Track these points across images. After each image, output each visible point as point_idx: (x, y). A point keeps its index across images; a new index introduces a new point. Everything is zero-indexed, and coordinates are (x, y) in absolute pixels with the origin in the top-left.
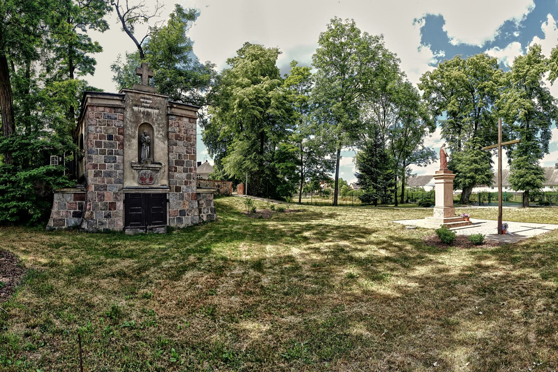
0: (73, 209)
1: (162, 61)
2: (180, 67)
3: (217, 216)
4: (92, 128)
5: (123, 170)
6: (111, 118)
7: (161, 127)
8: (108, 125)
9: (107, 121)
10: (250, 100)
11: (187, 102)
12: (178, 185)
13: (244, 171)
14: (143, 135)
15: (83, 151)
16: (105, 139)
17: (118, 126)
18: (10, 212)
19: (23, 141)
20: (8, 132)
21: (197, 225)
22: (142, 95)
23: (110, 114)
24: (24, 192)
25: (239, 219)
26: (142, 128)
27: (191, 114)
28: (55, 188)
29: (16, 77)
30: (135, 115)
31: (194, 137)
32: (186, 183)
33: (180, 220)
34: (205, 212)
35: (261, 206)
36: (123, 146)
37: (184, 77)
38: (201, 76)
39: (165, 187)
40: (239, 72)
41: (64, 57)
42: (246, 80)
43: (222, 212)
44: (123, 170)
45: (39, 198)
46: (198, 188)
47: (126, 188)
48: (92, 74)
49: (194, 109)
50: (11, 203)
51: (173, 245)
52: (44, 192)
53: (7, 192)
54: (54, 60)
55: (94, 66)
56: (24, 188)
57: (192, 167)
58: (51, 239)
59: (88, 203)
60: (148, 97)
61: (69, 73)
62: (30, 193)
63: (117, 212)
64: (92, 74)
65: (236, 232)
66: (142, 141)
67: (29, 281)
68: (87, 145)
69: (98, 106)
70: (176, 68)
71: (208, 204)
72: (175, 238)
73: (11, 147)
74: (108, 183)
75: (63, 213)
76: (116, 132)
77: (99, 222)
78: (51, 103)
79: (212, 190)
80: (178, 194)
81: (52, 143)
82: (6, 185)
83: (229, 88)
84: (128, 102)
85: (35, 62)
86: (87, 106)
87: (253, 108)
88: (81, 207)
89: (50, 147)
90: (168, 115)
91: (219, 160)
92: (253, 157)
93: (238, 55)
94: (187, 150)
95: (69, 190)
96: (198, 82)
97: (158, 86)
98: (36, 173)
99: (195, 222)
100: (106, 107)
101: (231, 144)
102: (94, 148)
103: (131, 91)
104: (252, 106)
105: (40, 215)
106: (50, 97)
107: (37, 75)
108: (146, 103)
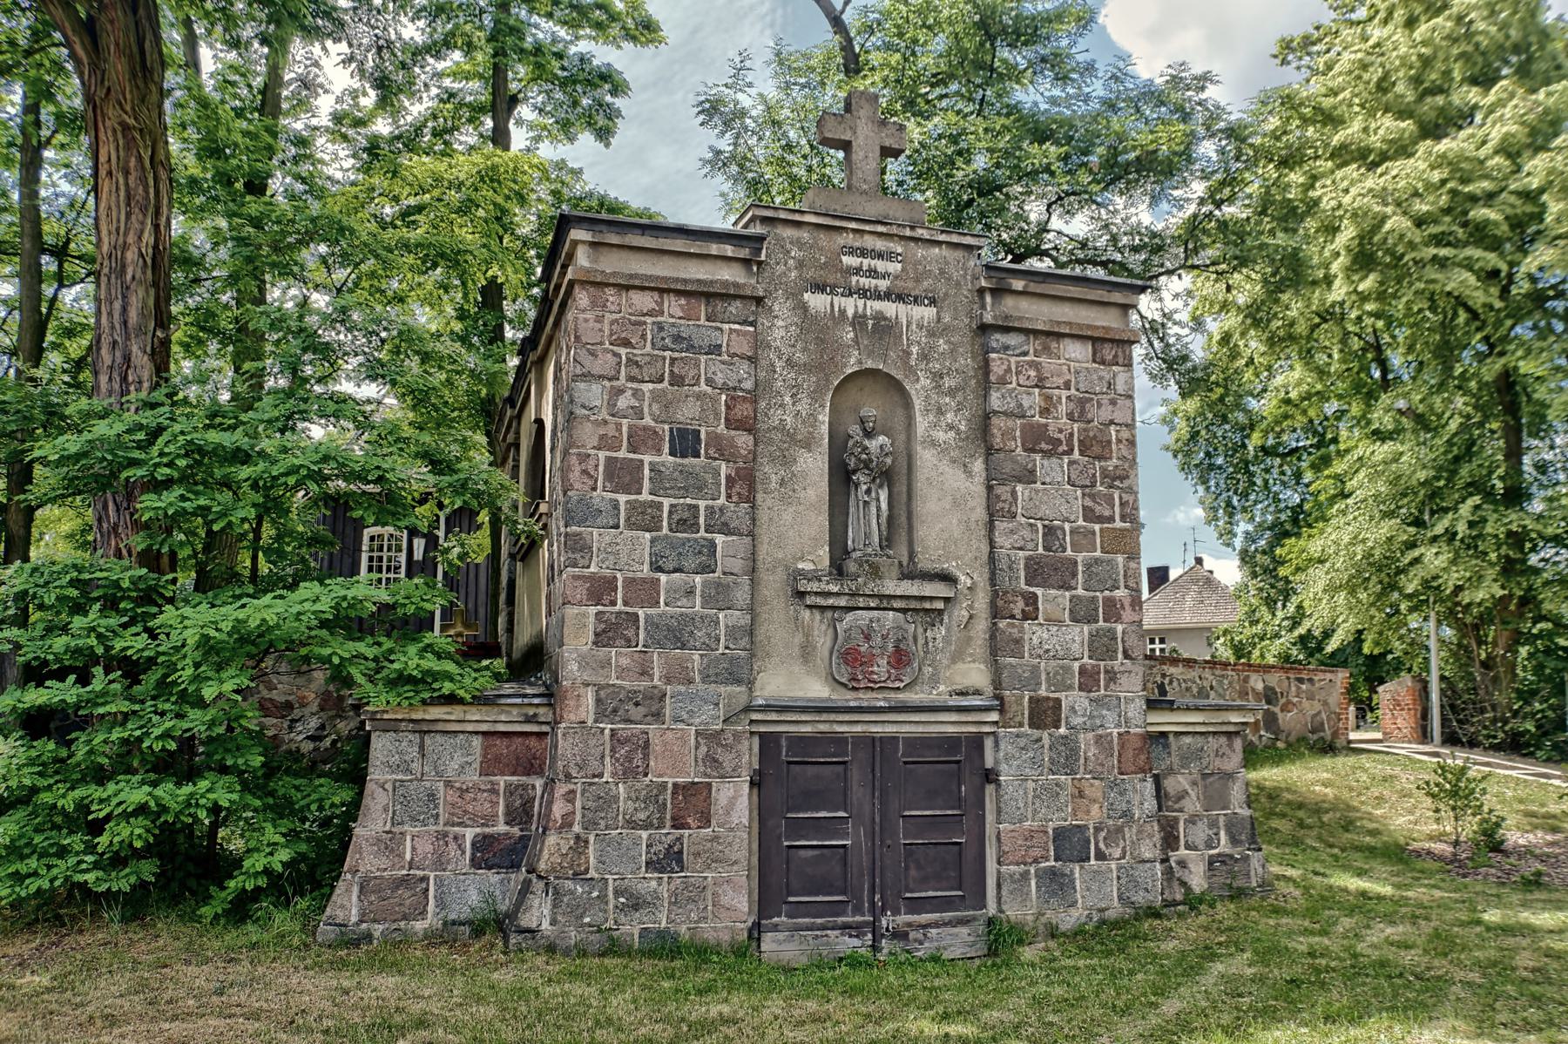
0: (475, 820)
1: (943, 83)
2: (1036, 104)
3: (1266, 864)
4: (593, 394)
5: (751, 610)
6: (689, 349)
7: (952, 392)
8: (677, 380)
9: (673, 360)
10: (1419, 222)
11: (1079, 262)
12: (1043, 692)
13: (1411, 610)
14: (855, 429)
15: (543, 508)
16: (659, 452)
17: (725, 388)
18: (103, 840)
19: (214, 436)
20: (124, 379)
21: (1153, 913)
22: (849, 239)
23: (686, 328)
24: (196, 720)
25: (1397, 886)
26: (853, 392)
27: (1103, 320)
28: (380, 701)
29: (204, 103)
30: (814, 329)
31: (1125, 434)
32: (1088, 680)
33: (1057, 884)
34: (1200, 843)
35: (1533, 815)
36: (752, 489)
37: (1057, 143)
38: (1139, 134)
39: (976, 701)
40: (1347, 94)
41: (469, 48)
42: (1388, 126)
43: (1297, 842)
44: (751, 610)
45: (280, 762)
46: (1152, 705)
47: (766, 708)
48: (604, 134)
49: (1117, 297)
50: (111, 787)
51: (1017, 1027)
52: (314, 723)
53: (84, 723)
54: (418, 53)
55: (618, 102)
56: (201, 704)
57: (1121, 593)
58: (346, 992)
59: (561, 789)
60: (880, 245)
61: (489, 123)
62: (230, 729)
63: (715, 839)
64: (604, 134)
65: (1383, 964)
66: (852, 463)
68: (565, 478)
69: (628, 288)
70: (1012, 110)
71: (1213, 798)
72: (1032, 984)
73: (134, 463)
74: (668, 680)
75: (416, 843)
76: (717, 415)
77: (617, 893)
78: (385, 257)
79: (1235, 718)
80: (1046, 741)
81: (376, 461)
82: (84, 679)
83: (1296, 177)
84: (781, 268)
85: (317, 45)
86: (571, 284)
87: (1441, 263)
88: (521, 813)
89: (361, 477)
90: (984, 329)
91: (1269, 551)
92: (1462, 529)
93: (1333, 15)
94: (1089, 503)
95: (456, 712)
96: (1128, 164)
97: (929, 193)
98: (272, 619)
99: (1140, 898)
100: (669, 291)
101: (1326, 461)
102: (601, 496)
103: (797, 217)
104: (1433, 251)
105: (284, 855)
106: (383, 225)
107: (325, 105)
108: (873, 273)
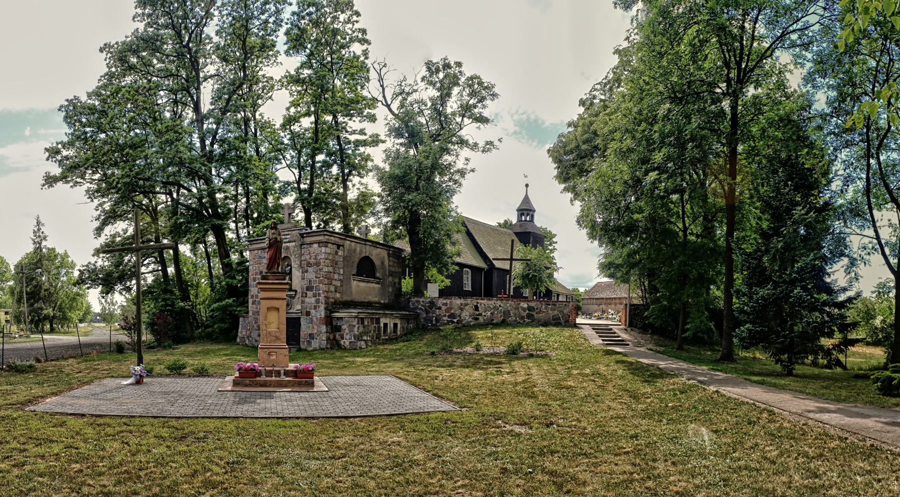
32: (315, 308)
33: (309, 343)
67: (404, 396)
71: (351, 331)
